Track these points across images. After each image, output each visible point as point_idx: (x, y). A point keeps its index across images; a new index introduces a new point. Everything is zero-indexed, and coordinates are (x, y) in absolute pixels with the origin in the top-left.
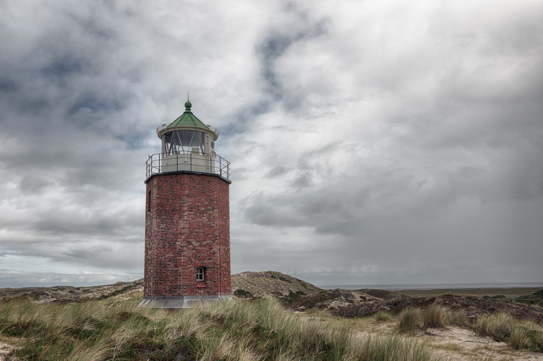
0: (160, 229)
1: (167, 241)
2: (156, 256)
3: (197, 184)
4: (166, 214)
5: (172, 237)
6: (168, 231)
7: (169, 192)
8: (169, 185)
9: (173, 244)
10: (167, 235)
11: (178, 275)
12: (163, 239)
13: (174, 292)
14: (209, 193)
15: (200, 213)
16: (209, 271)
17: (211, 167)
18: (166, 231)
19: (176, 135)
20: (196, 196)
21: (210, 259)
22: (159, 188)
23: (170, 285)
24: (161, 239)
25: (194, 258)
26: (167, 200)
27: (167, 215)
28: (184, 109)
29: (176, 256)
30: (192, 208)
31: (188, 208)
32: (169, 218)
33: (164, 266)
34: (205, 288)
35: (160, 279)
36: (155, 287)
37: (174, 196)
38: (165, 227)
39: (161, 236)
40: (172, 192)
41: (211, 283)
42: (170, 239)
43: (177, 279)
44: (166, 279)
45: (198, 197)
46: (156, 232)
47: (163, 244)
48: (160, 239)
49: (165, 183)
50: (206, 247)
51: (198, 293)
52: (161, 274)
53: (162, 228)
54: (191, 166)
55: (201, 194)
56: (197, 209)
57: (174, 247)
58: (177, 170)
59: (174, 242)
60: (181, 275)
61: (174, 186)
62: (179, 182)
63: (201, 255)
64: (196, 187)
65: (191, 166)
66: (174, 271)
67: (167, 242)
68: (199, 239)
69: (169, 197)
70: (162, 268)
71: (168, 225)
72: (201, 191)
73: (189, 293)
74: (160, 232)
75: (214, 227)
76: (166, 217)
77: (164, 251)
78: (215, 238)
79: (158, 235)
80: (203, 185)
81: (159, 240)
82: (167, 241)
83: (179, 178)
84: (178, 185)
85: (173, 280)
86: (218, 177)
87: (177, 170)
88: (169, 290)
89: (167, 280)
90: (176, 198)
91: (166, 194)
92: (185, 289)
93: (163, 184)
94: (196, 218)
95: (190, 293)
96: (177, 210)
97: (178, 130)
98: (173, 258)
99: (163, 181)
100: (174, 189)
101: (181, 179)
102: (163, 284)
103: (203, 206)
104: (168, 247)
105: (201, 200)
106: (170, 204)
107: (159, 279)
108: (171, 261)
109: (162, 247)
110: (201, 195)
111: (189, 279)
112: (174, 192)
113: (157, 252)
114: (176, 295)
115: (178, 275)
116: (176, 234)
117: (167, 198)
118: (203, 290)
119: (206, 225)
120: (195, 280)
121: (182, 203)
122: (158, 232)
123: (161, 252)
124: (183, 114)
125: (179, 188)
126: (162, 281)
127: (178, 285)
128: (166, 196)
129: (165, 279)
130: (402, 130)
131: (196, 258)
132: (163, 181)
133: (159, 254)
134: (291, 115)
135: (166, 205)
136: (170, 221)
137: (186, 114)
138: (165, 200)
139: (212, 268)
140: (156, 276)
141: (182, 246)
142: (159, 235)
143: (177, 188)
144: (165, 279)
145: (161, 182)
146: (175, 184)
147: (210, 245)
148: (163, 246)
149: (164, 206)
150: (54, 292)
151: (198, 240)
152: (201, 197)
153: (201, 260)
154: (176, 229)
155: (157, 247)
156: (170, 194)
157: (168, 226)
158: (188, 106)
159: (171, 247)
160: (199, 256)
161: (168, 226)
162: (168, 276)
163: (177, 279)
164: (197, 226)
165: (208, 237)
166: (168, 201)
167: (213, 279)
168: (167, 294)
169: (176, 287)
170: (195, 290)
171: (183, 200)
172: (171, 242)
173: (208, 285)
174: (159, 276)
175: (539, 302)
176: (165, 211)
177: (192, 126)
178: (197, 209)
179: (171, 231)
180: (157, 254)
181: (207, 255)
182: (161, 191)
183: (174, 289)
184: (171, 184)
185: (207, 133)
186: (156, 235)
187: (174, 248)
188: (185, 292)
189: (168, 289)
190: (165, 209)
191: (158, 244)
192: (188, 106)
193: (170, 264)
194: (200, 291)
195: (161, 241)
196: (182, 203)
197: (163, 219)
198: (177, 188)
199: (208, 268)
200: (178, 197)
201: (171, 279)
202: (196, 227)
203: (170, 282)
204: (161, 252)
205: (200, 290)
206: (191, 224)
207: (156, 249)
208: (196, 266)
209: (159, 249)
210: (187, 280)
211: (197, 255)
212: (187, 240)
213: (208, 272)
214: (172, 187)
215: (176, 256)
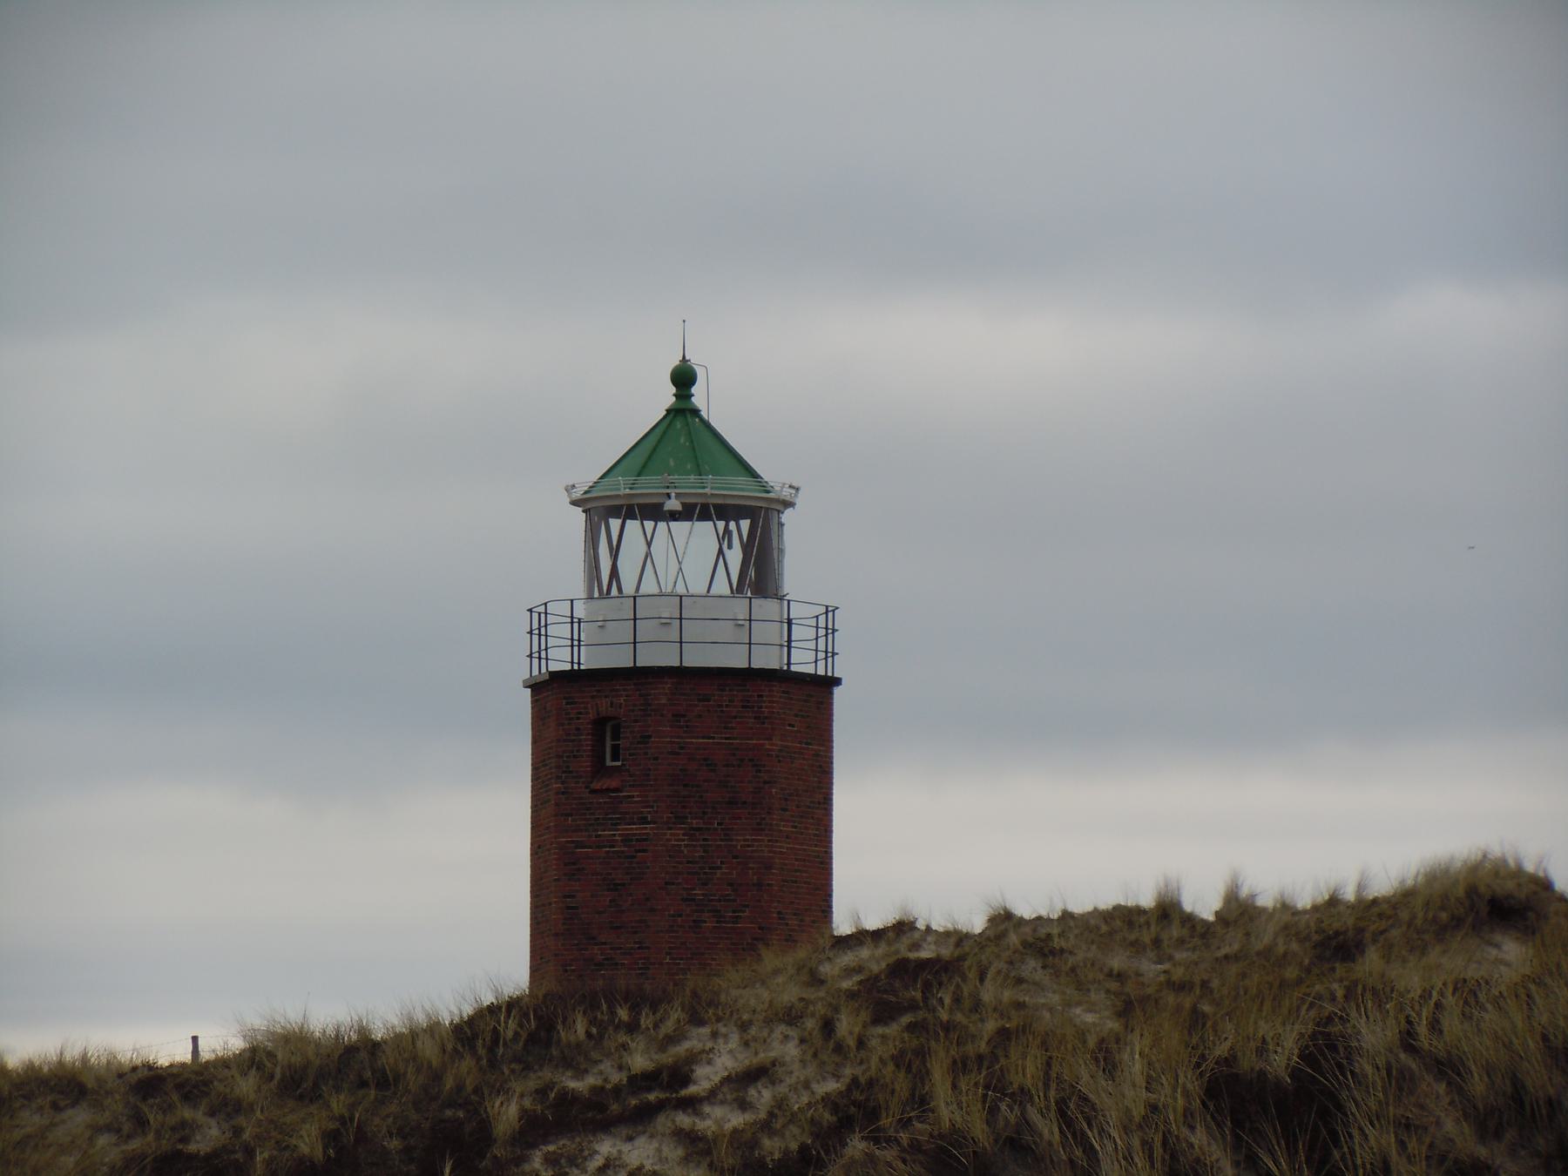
2: (667, 954)
4: (704, 813)
5: (728, 895)
17: (681, 619)
18: (705, 873)
28: (666, 396)
37: (734, 755)
49: (697, 706)
54: (681, 646)
58: (681, 664)
61: (735, 717)
62: (753, 707)
65: (681, 646)
79: (673, 884)
86: (784, 677)
87: (681, 664)
96: (745, 803)
97: (714, 506)
100: (732, 728)
101: (761, 696)
121: (765, 782)
124: (665, 417)
125: (752, 728)
130: (1002, 912)
135: (705, 781)
137: (675, 416)
142: (679, 884)
158: (683, 378)
180: (670, 948)
184: (722, 711)
186: (666, 883)
190: (701, 797)
191: (673, 916)
192: (683, 378)
196: (765, 782)
200: (750, 760)
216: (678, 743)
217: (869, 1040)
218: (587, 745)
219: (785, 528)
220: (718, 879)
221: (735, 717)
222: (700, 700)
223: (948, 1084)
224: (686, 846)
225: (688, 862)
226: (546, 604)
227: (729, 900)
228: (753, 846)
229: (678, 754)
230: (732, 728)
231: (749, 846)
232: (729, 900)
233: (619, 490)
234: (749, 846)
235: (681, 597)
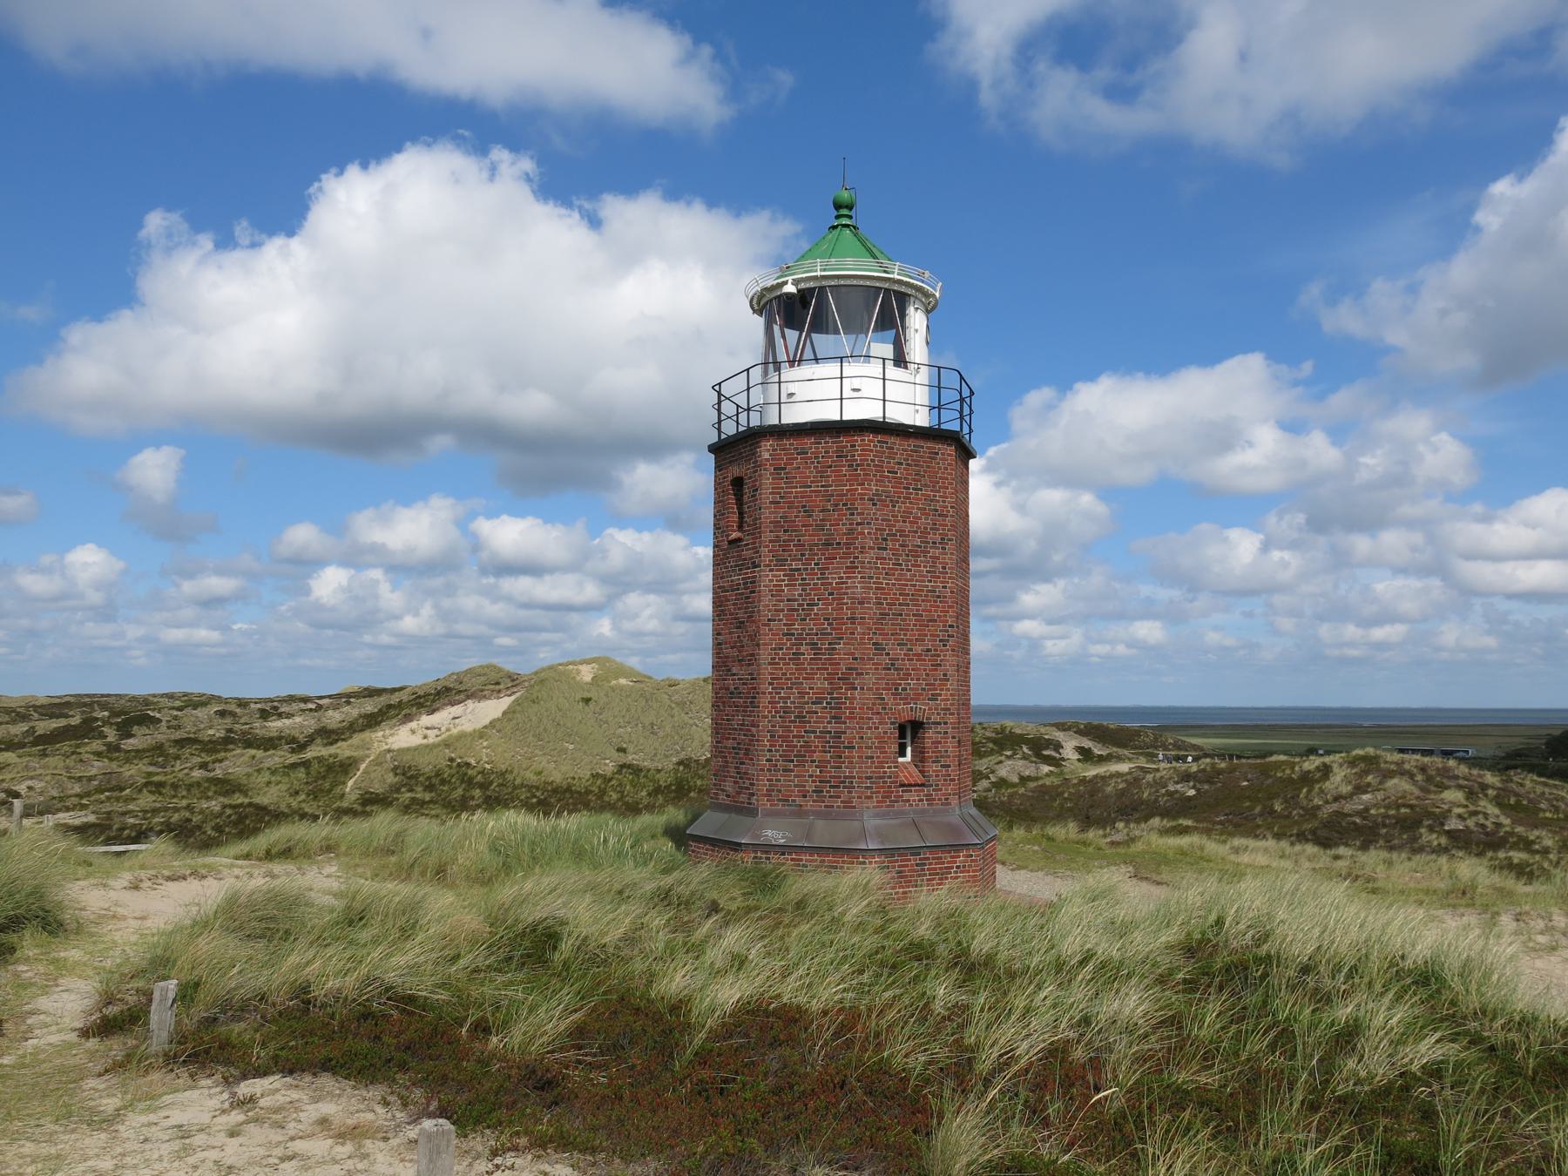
0: (782, 601)
1: (805, 639)
2: (770, 684)
3: (901, 464)
4: (803, 555)
6: (808, 610)
7: (810, 487)
8: (813, 463)
9: (827, 649)
10: (805, 620)
11: (845, 747)
12: (793, 634)
13: (830, 797)
14: (932, 491)
15: (908, 555)
16: (930, 734)
18: (803, 610)
19: (822, 305)
20: (897, 502)
21: (934, 698)
22: (778, 474)
23: (816, 776)
24: (788, 634)
25: (892, 694)
26: (805, 512)
27: (806, 559)
29: (837, 689)
30: (886, 540)
31: (877, 539)
32: (813, 569)
33: (795, 717)
34: (923, 785)
35: (785, 756)
36: (768, 780)
37: (830, 501)
38: (800, 595)
39: (785, 625)
40: (822, 486)
41: (937, 771)
42: (817, 634)
43: (841, 757)
44: (805, 756)
45: (902, 503)
46: (769, 611)
47: (792, 649)
48: (784, 635)
50: (925, 660)
51: (903, 801)
52: (787, 741)
53: (788, 600)
55: (911, 494)
56: (898, 541)
57: (830, 659)
59: (829, 644)
60: (854, 747)
61: (831, 467)
63: (909, 684)
64: (896, 473)
66: (830, 732)
67: (806, 644)
68: (905, 635)
69: (812, 501)
70: (790, 722)
71: (811, 589)
72: (911, 484)
73: (878, 802)
74: (783, 610)
75: (945, 597)
76: (803, 564)
77: (796, 669)
78: (948, 631)
80: (915, 465)
81: (778, 635)
82: (805, 639)
83: (847, 442)
84: (844, 466)
85: (829, 762)
88: (814, 791)
89: (807, 761)
90: (837, 505)
91: (801, 492)
92: (867, 788)
93: (790, 459)
94: (897, 570)
95: (882, 802)
96: (839, 544)
98: (828, 694)
99: (790, 449)
100: (828, 477)
102: (792, 771)
103: (916, 532)
104: (811, 659)
105: (911, 513)
106: (816, 525)
107: (780, 756)
108: (822, 703)
109: (789, 659)
110: (909, 498)
111: (878, 757)
112: (831, 486)
113: (772, 674)
114: (838, 807)
115: (845, 747)
116: (835, 619)
117: (805, 506)
118: (915, 791)
119: (923, 591)
120: (894, 762)
121: (858, 524)
122: (776, 610)
123: (786, 674)
125: (845, 475)
126: (793, 761)
127: (845, 777)
128: (802, 497)
129: (802, 756)
131: (896, 694)
132: (790, 449)
133: (781, 679)
134: (714, 211)
136: (818, 579)
138: (800, 512)
139: (939, 723)
140: (771, 746)
141: (856, 659)
143: (839, 476)
144: (802, 756)
145: (785, 455)
146: (832, 462)
147: (935, 655)
148: (793, 654)
149: (796, 531)
150: (175, 713)
151: (903, 639)
152: (910, 503)
153: (912, 699)
154: (837, 604)
155: (773, 659)
156: (815, 491)
157: (810, 594)
159: (821, 659)
160: (905, 689)
161: (810, 594)
162: (811, 747)
163: (841, 757)
164: (900, 594)
165: (929, 630)
166: (810, 516)
167: (942, 757)
168: (809, 801)
169: (840, 783)
170: (892, 792)
171: (858, 514)
172: (822, 644)
173: (928, 776)
174: (781, 746)
175: (1377, 757)
176: (800, 545)
177: (876, 274)
178: (898, 541)
179: (819, 610)
181: (927, 685)
182: (785, 483)
183: (830, 787)
185: (916, 298)
186: (769, 620)
187: (830, 664)
188: (867, 798)
189: (810, 786)
191: (775, 649)
193: (817, 713)
194: (906, 796)
195: (787, 640)
196: (858, 524)
197: (791, 570)
198: (839, 476)
199: (928, 723)
200: (843, 505)
201: (822, 756)
202: (899, 599)
203: (816, 767)
204: (786, 674)
205: (906, 791)
206: (884, 589)
207: (769, 664)
208: (896, 718)
209: (779, 664)
210: (873, 762)
211: (900, 684)
212: (872, 639)
213: (929, 738)
214: (823, 472)
215: (837, 689)
216: (780, 493)
217: (227, 1081)
218: (766, 493)
219: (751, 311)
220: (815, 614)
221: (831, 467)
222: (798, 454)
223: (1116, 762)
224: (786, 585)
225: (788, 600)
226: (748, 370)
227: (825, 634)
228: (847, 583)
229: (779, 503)
230: (828, 477)
231: (843, 583)
232: (825, 634)
233: (816, 271)
234: (843, 583)
235: (884, 359)
